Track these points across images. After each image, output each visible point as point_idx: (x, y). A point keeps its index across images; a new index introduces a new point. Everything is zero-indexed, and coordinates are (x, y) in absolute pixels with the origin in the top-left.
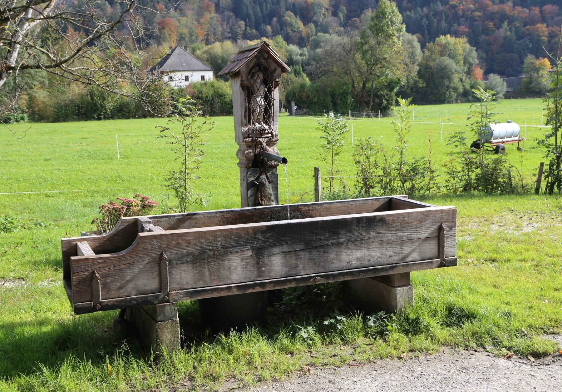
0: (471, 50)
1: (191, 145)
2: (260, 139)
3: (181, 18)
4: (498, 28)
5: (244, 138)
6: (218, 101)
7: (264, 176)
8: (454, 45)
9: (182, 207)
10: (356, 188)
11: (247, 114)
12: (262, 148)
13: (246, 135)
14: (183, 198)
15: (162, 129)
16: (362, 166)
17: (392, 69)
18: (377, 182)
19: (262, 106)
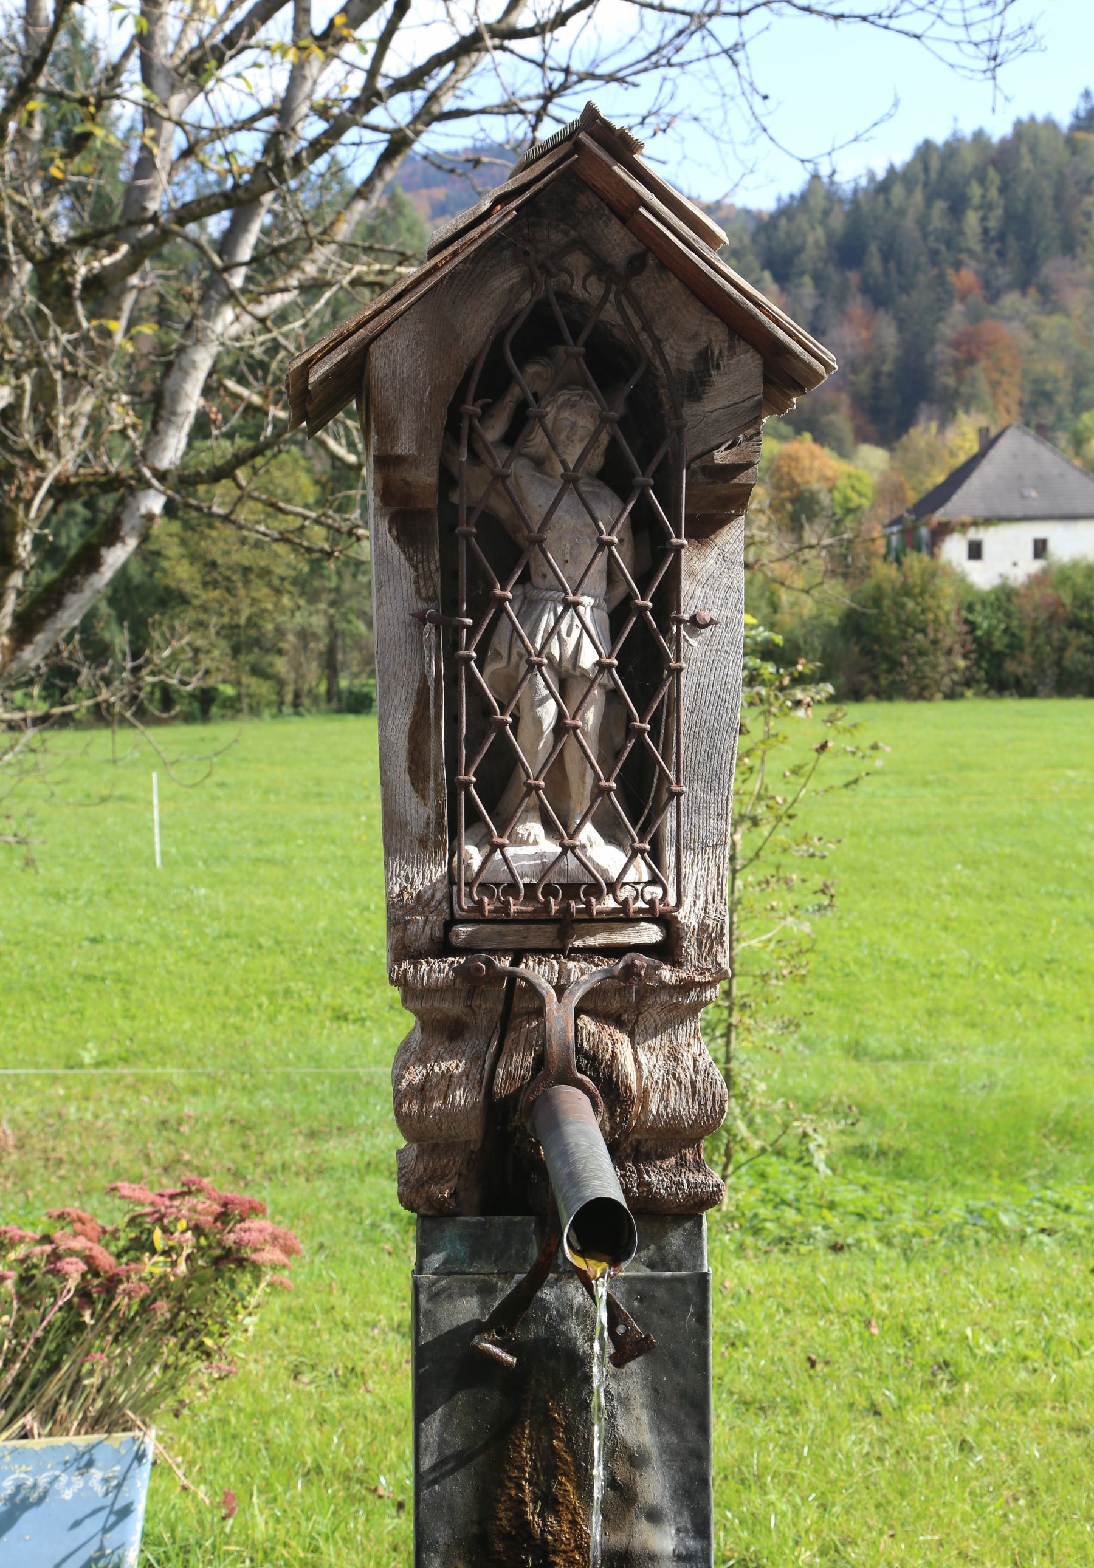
3: (1043, 319)
13: (423, 928)
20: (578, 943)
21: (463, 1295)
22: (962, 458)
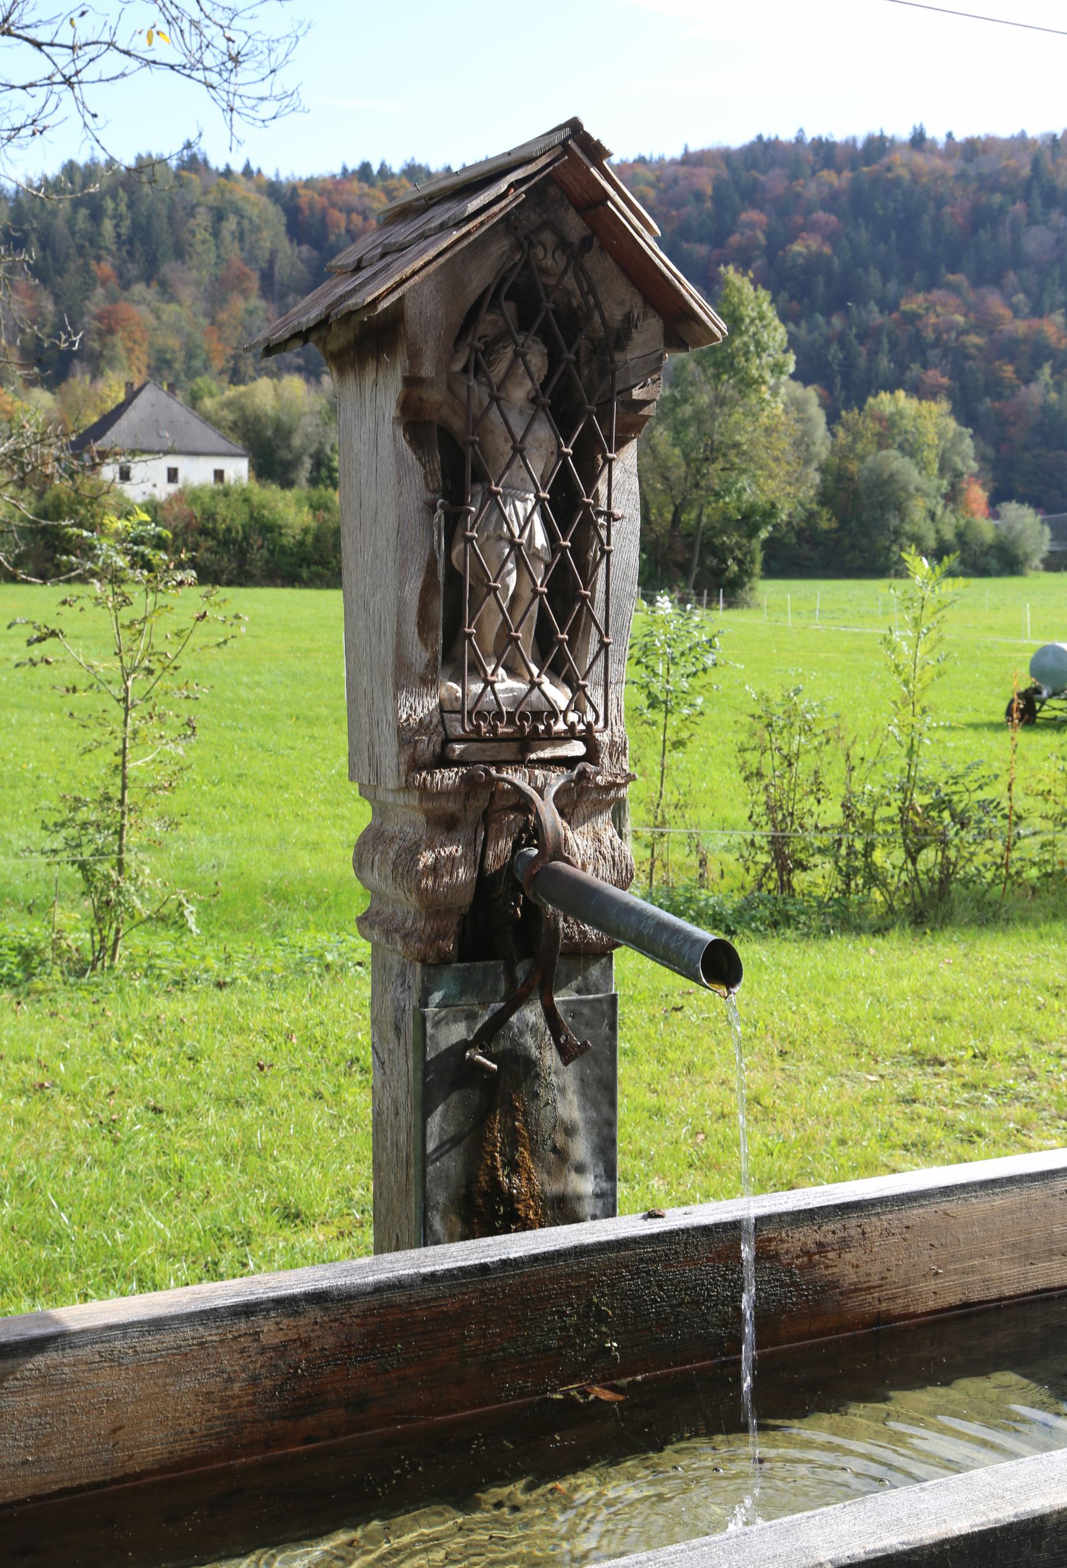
0: (961, 434)
1: (146, 699)
2: (517, 777)
3: (163, 306)
4: (1027, 381)
5: (416, 765)
6: (260, 542)
7: (532, 1014)
8: (915, 420)
9: (105, 933)
10: (748, 870)
11: (438, 608)
12: (535, 833)
13: (427, 746)
14: (108, 903)
15: (36, 634)
16: (766, 788)
17: (754, 476)
18: (820, 850)
19: (536, 555)
20: (533, 756)
21: (455, 1021)
22: (110, 406)
